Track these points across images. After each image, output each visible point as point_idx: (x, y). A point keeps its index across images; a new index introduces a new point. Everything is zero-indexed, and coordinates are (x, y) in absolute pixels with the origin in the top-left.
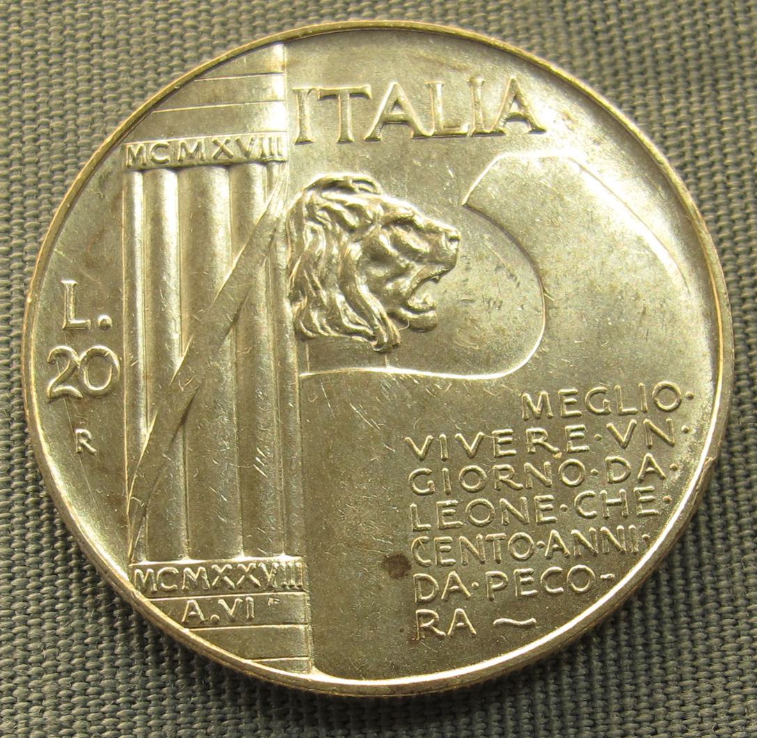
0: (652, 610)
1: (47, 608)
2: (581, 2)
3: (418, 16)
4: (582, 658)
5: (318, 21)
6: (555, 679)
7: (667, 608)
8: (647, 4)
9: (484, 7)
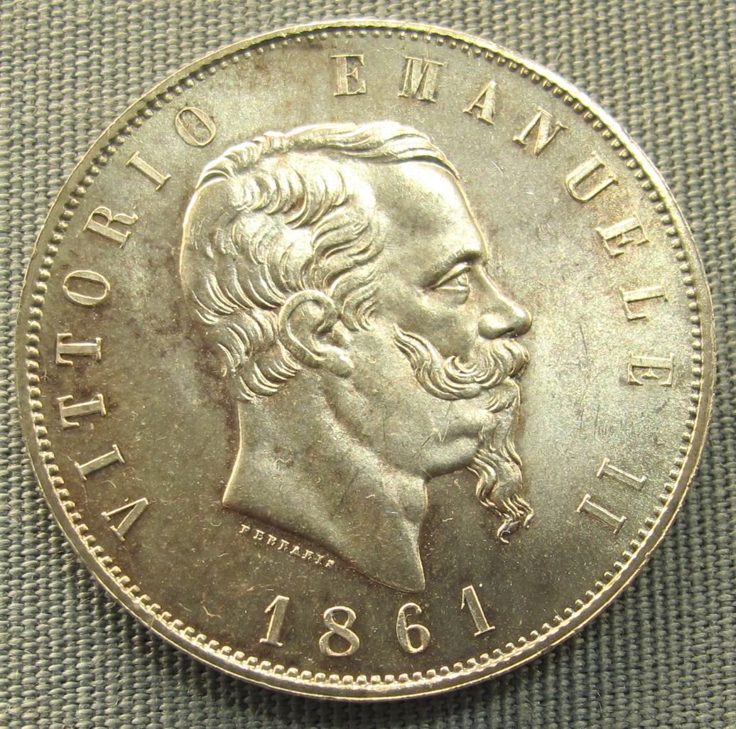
0: (579, 663)
1: (15, 530)
2: (611, 3)
3: (388, 14)
4: (565, 659)
5: (308, 21)
6: (486, 718)
7: (647, 622)
8: (311, 3)
9: (593, 7)
